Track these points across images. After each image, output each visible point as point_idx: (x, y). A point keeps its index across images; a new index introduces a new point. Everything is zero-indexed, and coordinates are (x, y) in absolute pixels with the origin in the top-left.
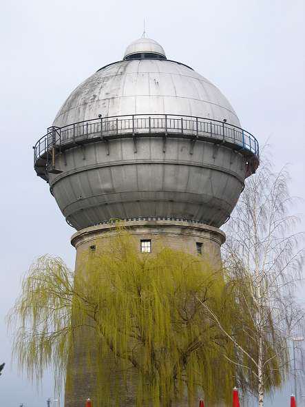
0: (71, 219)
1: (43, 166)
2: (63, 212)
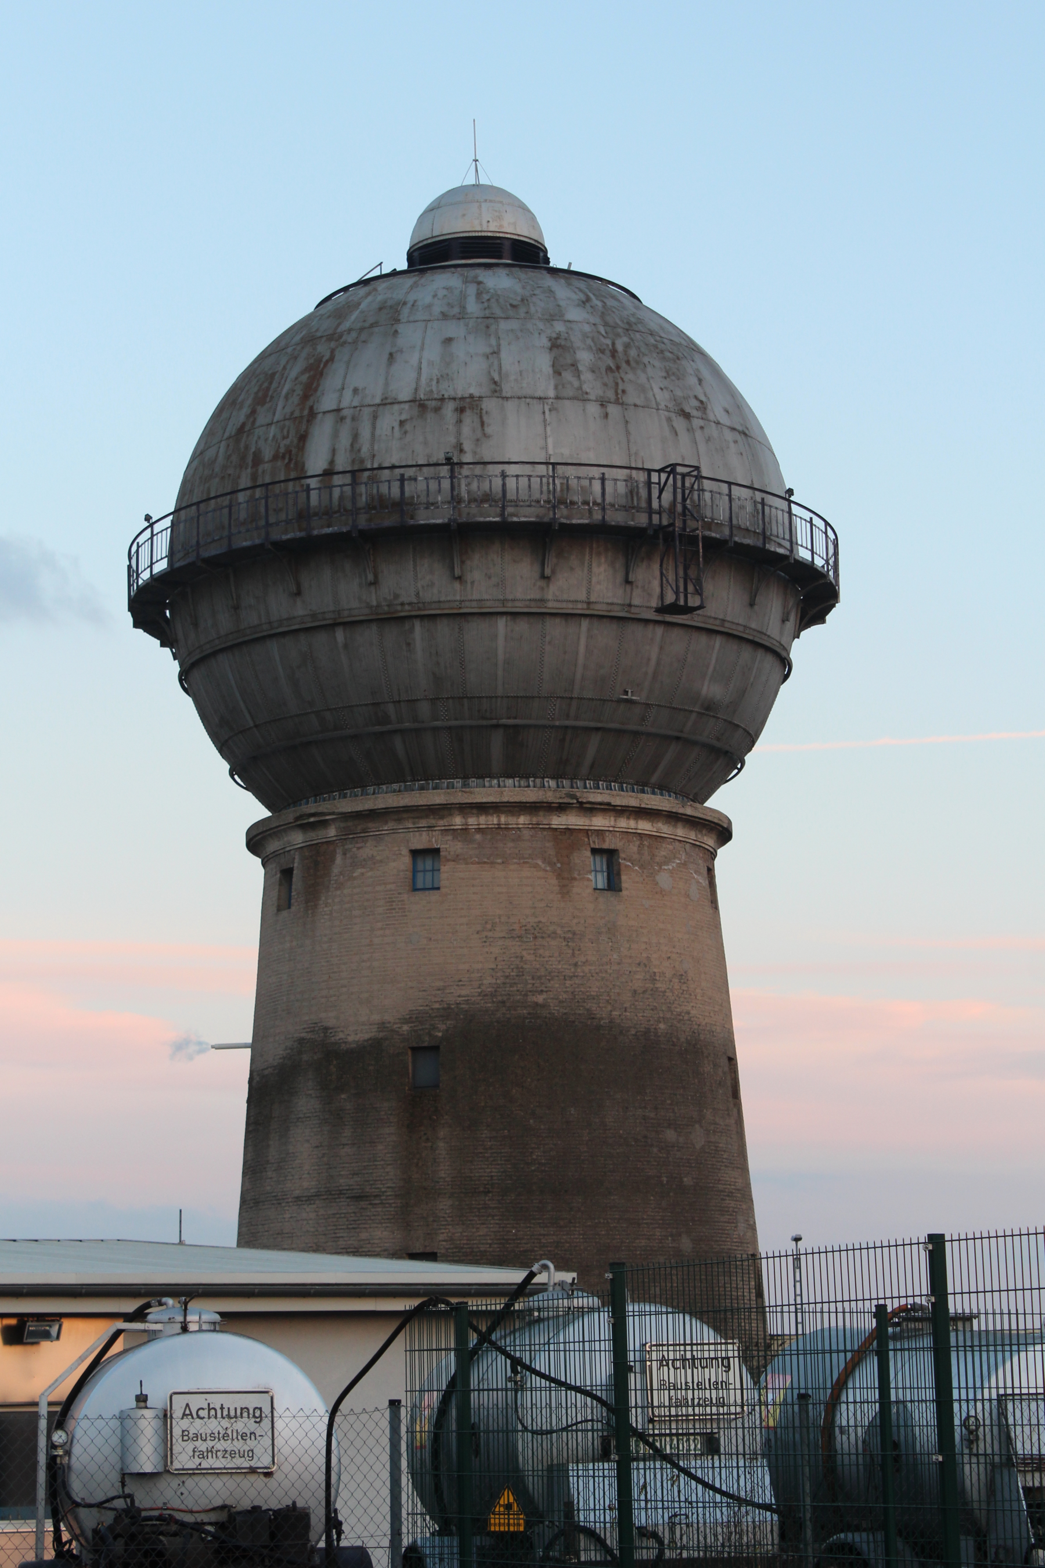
0: (247, 769)
1: (152, 606)
2: (223, 747)
